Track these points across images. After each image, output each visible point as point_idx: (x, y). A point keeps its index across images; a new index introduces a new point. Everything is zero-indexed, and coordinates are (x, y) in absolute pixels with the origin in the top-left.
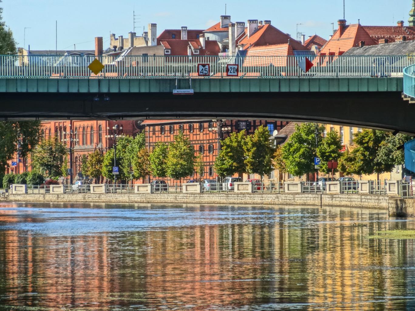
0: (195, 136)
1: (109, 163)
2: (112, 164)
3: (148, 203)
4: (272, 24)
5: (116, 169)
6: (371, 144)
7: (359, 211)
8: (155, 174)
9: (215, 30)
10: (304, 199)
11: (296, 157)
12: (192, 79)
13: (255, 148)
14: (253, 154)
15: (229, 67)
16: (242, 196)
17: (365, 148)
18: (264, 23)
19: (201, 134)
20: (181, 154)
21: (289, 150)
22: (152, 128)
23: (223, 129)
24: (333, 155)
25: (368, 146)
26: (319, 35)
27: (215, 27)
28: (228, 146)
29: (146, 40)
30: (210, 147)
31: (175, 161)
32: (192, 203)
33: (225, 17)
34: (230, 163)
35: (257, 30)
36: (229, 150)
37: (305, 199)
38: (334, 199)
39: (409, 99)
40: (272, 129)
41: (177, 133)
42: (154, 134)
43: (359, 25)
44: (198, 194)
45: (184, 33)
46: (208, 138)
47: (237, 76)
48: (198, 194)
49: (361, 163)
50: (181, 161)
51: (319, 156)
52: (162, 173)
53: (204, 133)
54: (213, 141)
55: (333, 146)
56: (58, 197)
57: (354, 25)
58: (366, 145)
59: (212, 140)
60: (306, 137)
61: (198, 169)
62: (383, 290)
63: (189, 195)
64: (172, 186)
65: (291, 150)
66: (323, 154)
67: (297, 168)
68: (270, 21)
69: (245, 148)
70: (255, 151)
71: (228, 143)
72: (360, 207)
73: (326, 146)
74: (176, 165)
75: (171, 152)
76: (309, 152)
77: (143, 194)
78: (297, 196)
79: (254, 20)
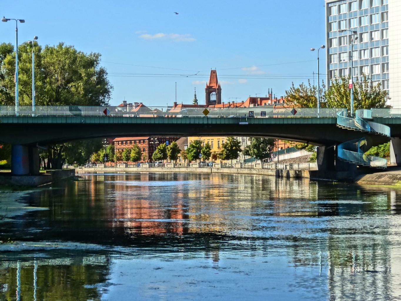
2: (104, 156)
4: (143, 104)
5: (106, 158)
7: (236, 175)
17: (227, 150)
19: (140, 145)
20: (136, 152)
28: (159, 149)
30: (143, 150)
31: (134, 155)
33: (126, 102)
39: (342, 127)
42: (118, 144)
43: (182, 104)
49: (225, 156)
50: (136, 155)
57: (180, 104)
61: (142, 158)
70: (172, 151)
71: (159, 148)
74: (135, 156)
75: (133, 151)
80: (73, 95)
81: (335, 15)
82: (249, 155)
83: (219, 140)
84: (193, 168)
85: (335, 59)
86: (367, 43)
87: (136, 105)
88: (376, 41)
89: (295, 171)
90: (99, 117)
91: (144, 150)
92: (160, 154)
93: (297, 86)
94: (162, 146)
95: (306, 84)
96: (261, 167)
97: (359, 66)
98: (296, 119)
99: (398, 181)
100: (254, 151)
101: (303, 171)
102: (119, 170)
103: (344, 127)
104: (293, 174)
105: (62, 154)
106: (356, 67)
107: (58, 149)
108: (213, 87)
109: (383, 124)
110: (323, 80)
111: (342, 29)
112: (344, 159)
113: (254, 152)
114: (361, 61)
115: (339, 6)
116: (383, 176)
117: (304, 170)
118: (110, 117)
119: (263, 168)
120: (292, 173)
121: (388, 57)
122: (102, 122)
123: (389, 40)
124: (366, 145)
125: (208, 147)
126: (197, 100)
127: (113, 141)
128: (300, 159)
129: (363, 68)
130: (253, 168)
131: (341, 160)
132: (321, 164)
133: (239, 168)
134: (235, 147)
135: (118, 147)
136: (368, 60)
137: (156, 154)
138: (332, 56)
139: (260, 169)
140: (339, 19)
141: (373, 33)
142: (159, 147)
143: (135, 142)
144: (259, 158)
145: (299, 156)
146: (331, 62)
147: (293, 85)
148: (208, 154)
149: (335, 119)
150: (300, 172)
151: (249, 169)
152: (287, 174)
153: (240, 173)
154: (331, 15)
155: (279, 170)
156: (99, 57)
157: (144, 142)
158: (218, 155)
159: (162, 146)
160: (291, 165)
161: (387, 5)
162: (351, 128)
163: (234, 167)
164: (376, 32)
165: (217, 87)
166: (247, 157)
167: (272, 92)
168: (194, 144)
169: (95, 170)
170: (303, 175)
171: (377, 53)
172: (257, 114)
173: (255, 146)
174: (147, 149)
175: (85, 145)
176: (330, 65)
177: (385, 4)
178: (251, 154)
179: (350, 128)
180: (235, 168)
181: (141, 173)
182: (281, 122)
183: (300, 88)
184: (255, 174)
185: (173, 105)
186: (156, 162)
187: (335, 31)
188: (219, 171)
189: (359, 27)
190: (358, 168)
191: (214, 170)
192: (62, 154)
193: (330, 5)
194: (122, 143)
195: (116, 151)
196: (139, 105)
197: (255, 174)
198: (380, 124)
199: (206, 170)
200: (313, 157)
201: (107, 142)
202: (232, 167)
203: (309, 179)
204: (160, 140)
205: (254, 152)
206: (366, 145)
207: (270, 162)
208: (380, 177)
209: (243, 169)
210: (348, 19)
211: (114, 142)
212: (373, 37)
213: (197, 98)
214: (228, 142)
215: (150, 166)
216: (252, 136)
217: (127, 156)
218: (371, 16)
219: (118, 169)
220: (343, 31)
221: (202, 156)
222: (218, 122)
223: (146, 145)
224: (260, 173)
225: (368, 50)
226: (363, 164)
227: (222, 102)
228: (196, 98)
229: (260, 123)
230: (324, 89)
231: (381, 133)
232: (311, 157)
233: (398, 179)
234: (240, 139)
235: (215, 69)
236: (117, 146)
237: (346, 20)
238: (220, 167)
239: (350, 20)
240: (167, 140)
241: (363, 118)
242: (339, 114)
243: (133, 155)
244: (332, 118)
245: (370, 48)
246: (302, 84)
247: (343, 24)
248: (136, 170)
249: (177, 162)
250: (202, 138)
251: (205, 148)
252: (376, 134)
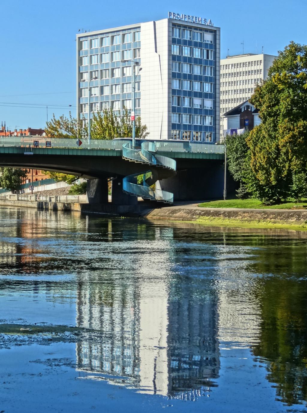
15: (47, 143)
39: (129, 160)
62: (123, 290)
81: (86, 49)
85: (86, 93)
86: (118, 79)
88: (128, 77)
89: (64, 204)
93: (58, 118)
96: (16, 199)
97: (110, 101)
99: (199, 217)
100: (6, 182)
101: (72, 204)
103: (131, 160)
104: (61, 207)
106: (107, 102)
109: (171, 158)
111: (125, 59)
113: (6, 184)
114: (112, 95)
115: (91, 40)
116: (177, 211)
117: (74, 203)
119: (18, 200)
120: (60, 206)
121: (140, 93)
123: (141, 76)
124: (152, 178)
128: (57, 191)
129: (114, 103)
130: (7, 200)
136: (119, 95)
138: (83, 90)
139: (16, 201)
140: (91, 54)
141: (125, 69)
144: (10, 189)
146: (81, 96)
147: (54, 116)
149: (121, 152)
150: (69, 204)
151: (3, 201)
154: (82, 49)
155: (42, 203)
161: (140, 42)
162: (138, 161)
164: (127, 68)
167: (5, 125)
170: (72, 208)
171: (128, 89)
172: (42, 144)
173: (7, 178)
176: (81, 99)
177: (137, 40)
178: (3, 185)
179: (138, 161)
182: (67, 153)
183: (60, 120)
187: (86, 65)
189: (110, 62)
190: (140, 202)
193: (81, 40)
198: (167, 158)
200: (72, 189)
205: (6, 184)
206: (152, 178)
207: (22, 193)
208: (174, 212)
210: (99, 54)
212: (124, 73)
216: (3, 166)
218: (123, 52)
220: (125, 61)
224: (16, 205)
225: (120, 86)
226: (150, 198)
229: (45, 154)
231: (169, 166)
232: (69, 189)
233: (198, 215)
237: (97, 55)
239: (101, 55)
241: (148, 151)
242: (124, 146)
245: (111, 84)
246: (62, 116)
247: (94, 58)
252: (164, 168)
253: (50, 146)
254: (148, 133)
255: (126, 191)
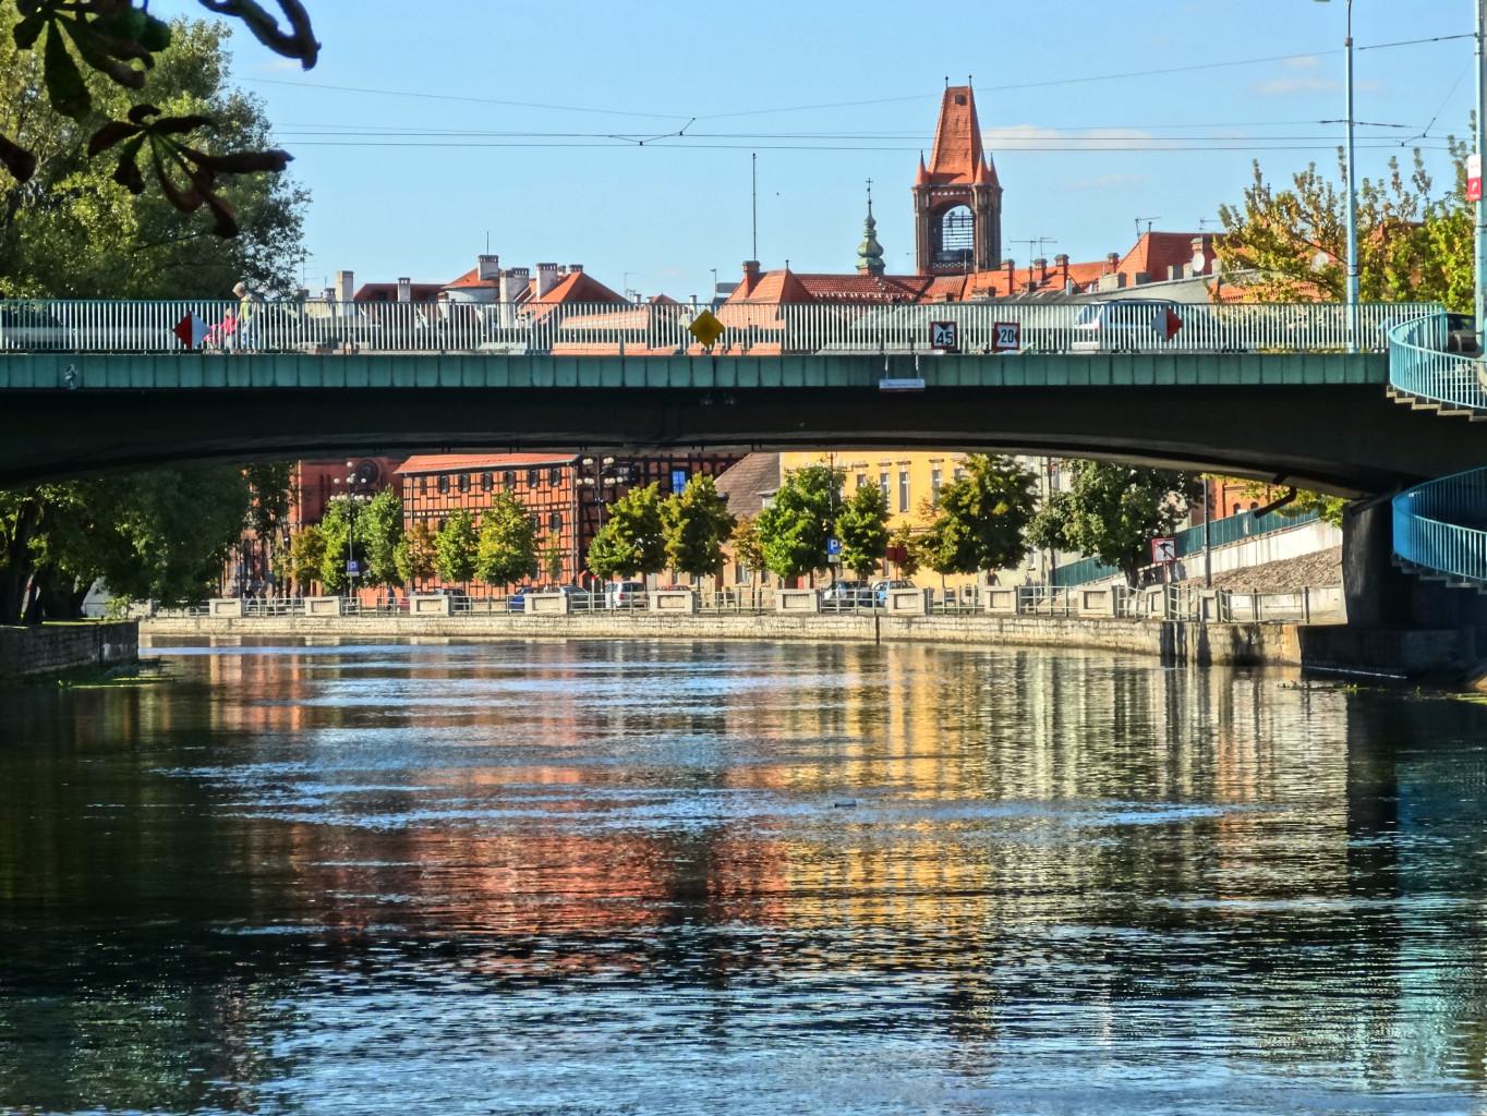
0: (472, 499)
1: (339, 553)
2: (344, 556)
3: (445, 635)
4: (585, 271)
5: (352, 564)
6: (975, 510)
8: (449, 574)
9: (468, 285)
10: (830, 625)
11: (787, 539)
12: (921, 357)
13: (686, 521)
14: (683, 531)
15: (1000, 329)
16: (669, 619)
18: (568, 271)
19: (533, 492)
20: (508, 534)
21: (773, 522)
22: (418, 480)
23: (607, 481)
24: (870, 533)
25: (968, 512)
26: (667, 294)
27: (465, 278)
28: (624, 517)
29: (331, 301)
30: (552, 518)
31: (496, 547)
32: (549, 636)
33: (488, 260)
34: (628, 552)
35: (556, 284)
36: (626, 524)
37: (834, 625)
38: (914, 626)
39: (1413, 400)
40: (683, 482)
41: (499, 489)
42: (424, 492)
44: (564, 616)
45: (404, 291)
46: (548, 501)
47: (1018, 348)
48: (564, 616)
50: (510, 549)
51: (841, 536)
52: (465, 572)
53: (540, 489)
54: (561, 506)
55: (870, 514)
56: (230, 624)
57: (775, 273)
58: (964, 511)
59: (558, 504)
60: (808, 496)
61: (544, 564)
63: (541, 619)
64: (480, 601)
65: (777, 524)
66: (849, 532)
67: (790, 562)
68: (581, 267)
69: (664, 519)
70: (686, 526)
71: (624, 510)
72: (996, 643)
73: (854, 514)
74: (498, 556)
76: (813, 527)
77: (430, 616)
78: (811, 619)
79: (549, 265)
80: (79, 232)
82: (1063, 544)
83: (936, 466)
84: (790, 615)
87: (549, 274)
90: (157, 356)
91: (555, 523)
92: (631, 540)
93: (1280, 184)
94: (640, 498)
95: (1329, 173)
96: (1109, 611)
98: (1178, 359)
100: (1087, 523)
102: (415, 629)
103: (1420, 400)
105: (33, 543)
107: (13, 517)
108: (954, 176)
110: (1417, 151)
112: (1419, 566)
113: (1088, 533)
118: (206, 361)
119: (1120, 615)
120: (1221, 639)
122: (166, 380)
125: (873, 504)
126: (880, 250)
127: (401, 470)
131: (1406, 571)
132: (1358, 590)
133: (1008, 616)
134: (1008, 502)
135: (425, 503)
137: (609, 544)
139: (1108, 620)
142: (621, 505)
143: (509, 480)
145: (1310, 551)
148: (872, 539)
149: (1382, 360)
151: (1053, 622)
152: (1200, 642)
153: (1014, 644)
156: (220, 40)
157: (555, 478)
158: (919, 548)
159: (638, 498)
160: (1224, 600)
162: (1451, 407)
163: (988, 609)
165: (978, 181)
166: (1066, 559)
168: (801, 491)
169: (293, 626)
174: (570, 517)
175: (147, 499)
180: (992, 615)
181: (529, 640)
183: (1295, 191)
184: (1077, 646)
185: (739, 276)
186: (608, 583)
188: (915, 632)
191: (891, 628)
192: (33, 543)
194: (443, 485)
195: (410, 527)
196: (564, 279)
197: (1077, 646)
199: (851, 627)
201: (358, 478)
202: (978, 611)
203: (1298, 671)
204: (641, 465)
205: (1088, 533)
209: (1024, 622)
211: (402, 475)
213: (879, 239)
214: (970, 476)
215: (576, 606)
217: (461, 554)
219: (410, 624)
221: (839, 550)
222: (659, 380)
223: (564, 495)
224: (1102, 641)
227: (1005, 256)
228: (872, 235)
229: (986, 383)
230: (1422, 197)
234: (1031, 463)
235: (965, 83)
236: (418, 502)
238: (921, 610)
240: (679, 469)
242: (1398, 336)
243: (488, 548)
244: (1368, 358)
246: (1307, 169)
248: (502, 629)
249: (726, 583)
250: (844, 459)
251: (858, 509)
253: (1014, 344)
254: (858, 267)
255: (1404, 560)
